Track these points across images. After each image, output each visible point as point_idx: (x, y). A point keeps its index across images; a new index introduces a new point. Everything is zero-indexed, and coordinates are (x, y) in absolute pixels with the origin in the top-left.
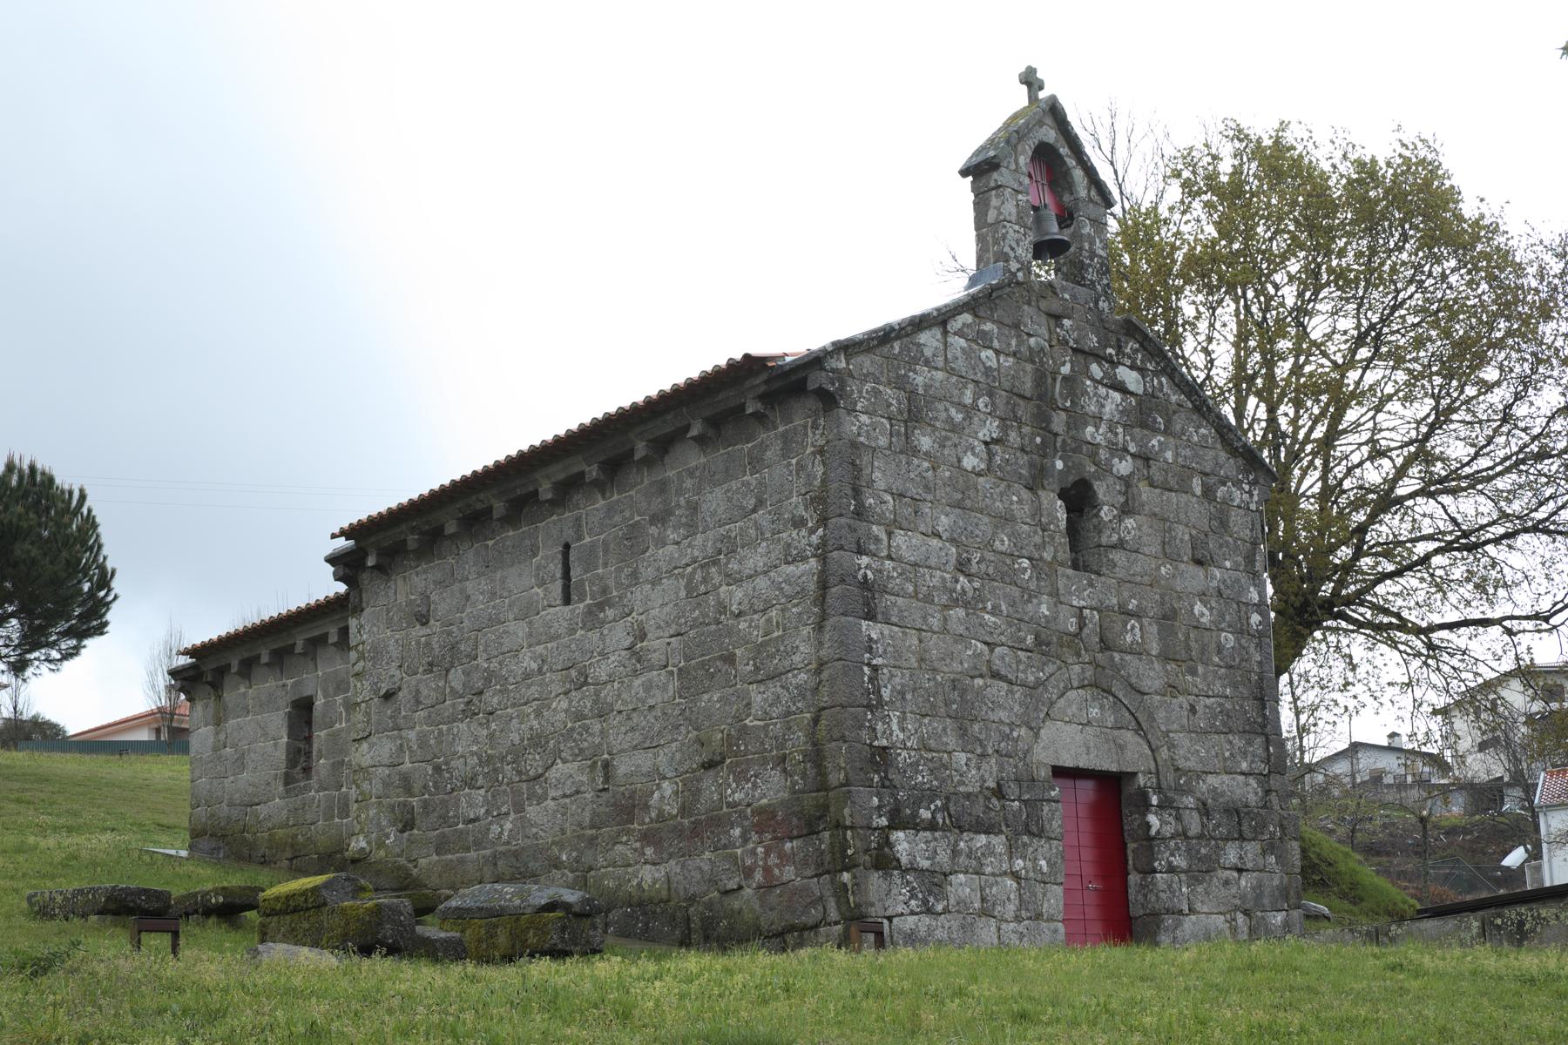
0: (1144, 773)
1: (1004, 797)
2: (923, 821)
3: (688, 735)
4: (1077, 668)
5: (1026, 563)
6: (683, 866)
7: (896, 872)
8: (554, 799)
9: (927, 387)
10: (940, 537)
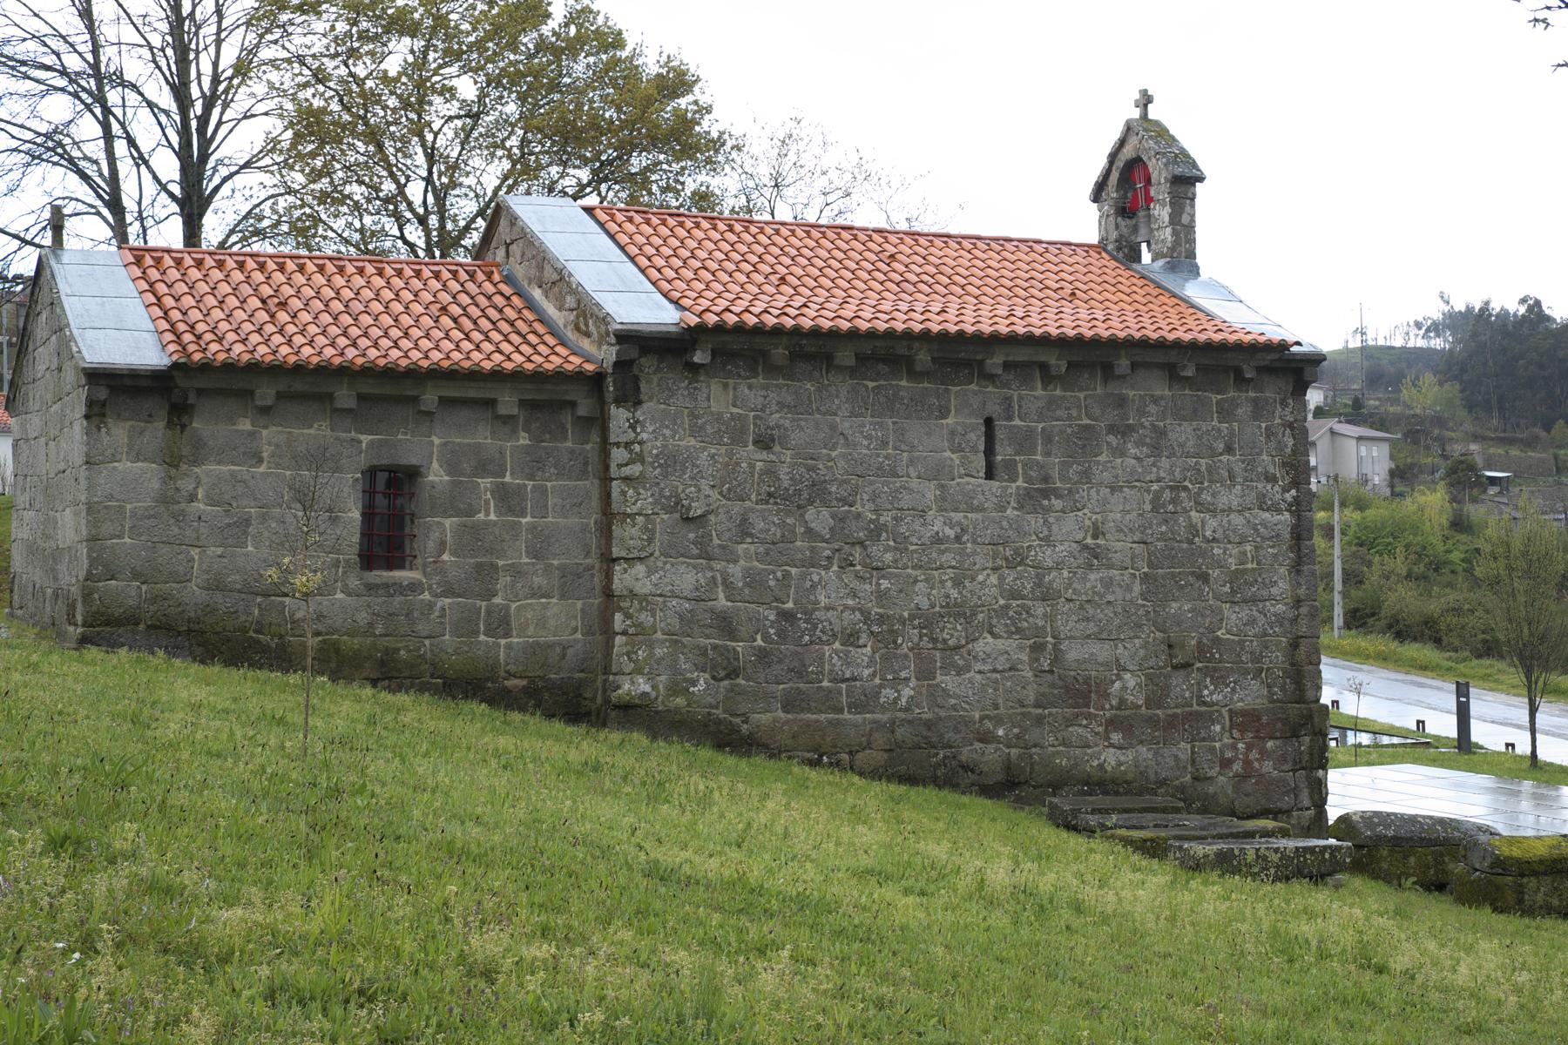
3: (1151, 635)
6: (1156, 753)
8: (980, 672)
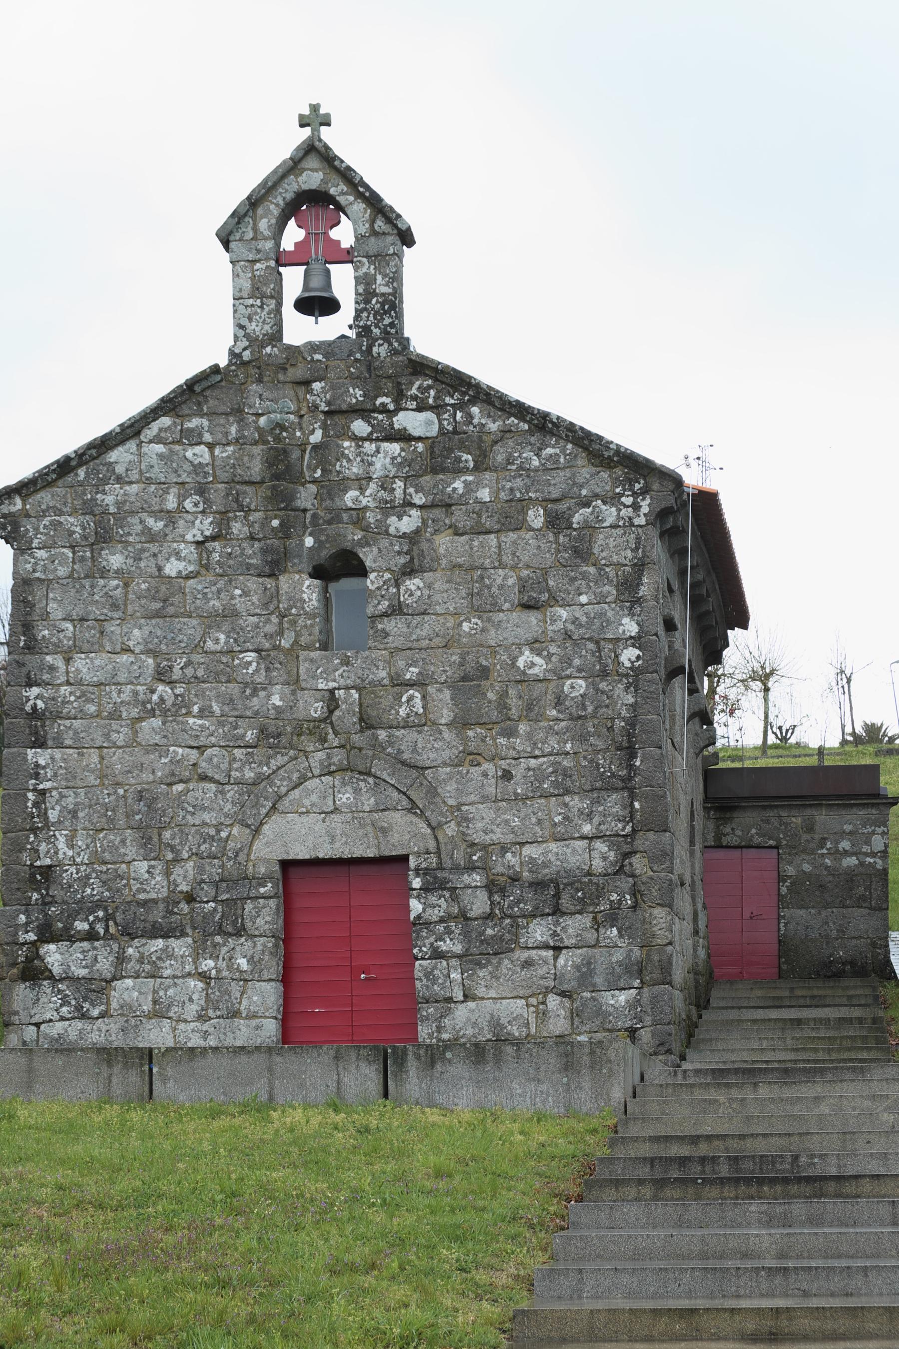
0: (418, 854)
1: (194, 900)
2: (79, 932)
4: (321, 755)
5: (251, 656)
7: (45, 983)
9: (119, 504)
10: (133, 652)
